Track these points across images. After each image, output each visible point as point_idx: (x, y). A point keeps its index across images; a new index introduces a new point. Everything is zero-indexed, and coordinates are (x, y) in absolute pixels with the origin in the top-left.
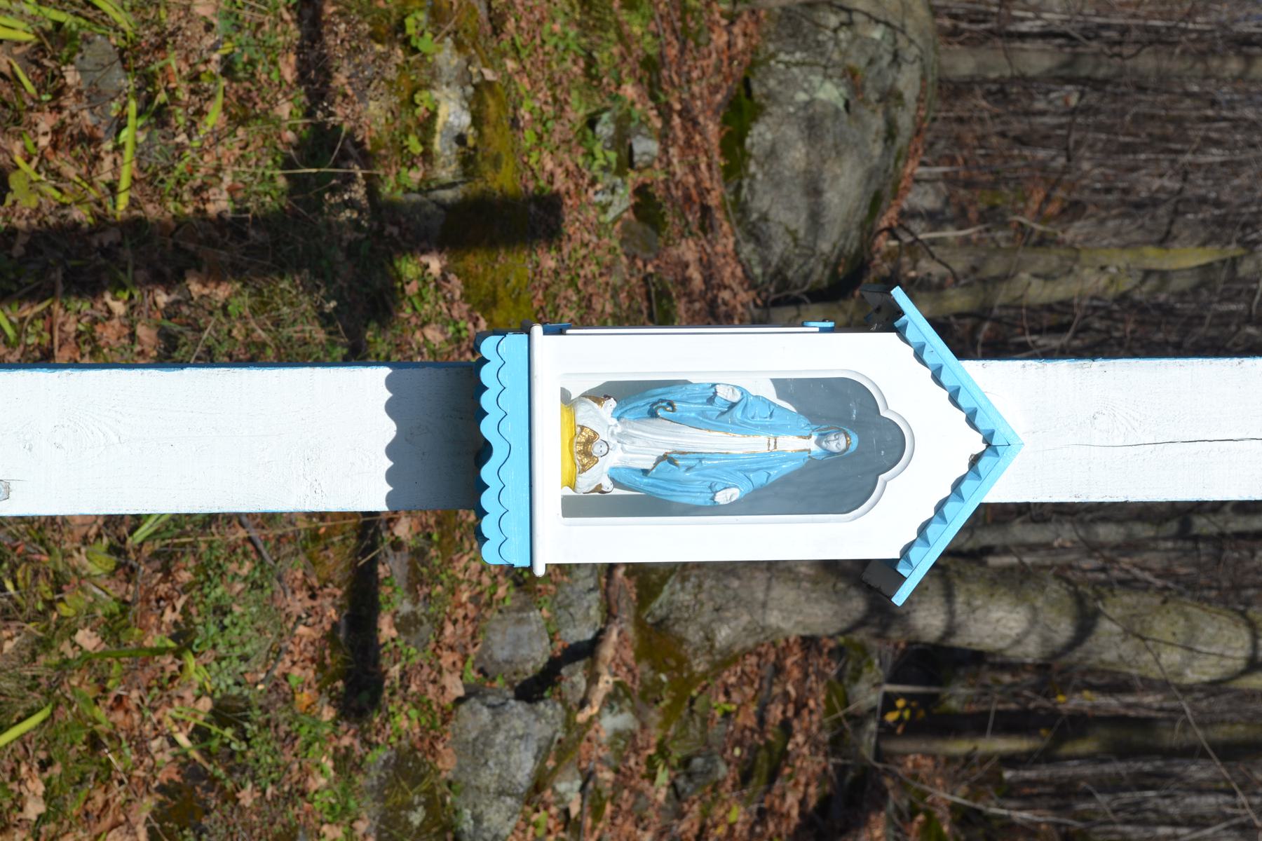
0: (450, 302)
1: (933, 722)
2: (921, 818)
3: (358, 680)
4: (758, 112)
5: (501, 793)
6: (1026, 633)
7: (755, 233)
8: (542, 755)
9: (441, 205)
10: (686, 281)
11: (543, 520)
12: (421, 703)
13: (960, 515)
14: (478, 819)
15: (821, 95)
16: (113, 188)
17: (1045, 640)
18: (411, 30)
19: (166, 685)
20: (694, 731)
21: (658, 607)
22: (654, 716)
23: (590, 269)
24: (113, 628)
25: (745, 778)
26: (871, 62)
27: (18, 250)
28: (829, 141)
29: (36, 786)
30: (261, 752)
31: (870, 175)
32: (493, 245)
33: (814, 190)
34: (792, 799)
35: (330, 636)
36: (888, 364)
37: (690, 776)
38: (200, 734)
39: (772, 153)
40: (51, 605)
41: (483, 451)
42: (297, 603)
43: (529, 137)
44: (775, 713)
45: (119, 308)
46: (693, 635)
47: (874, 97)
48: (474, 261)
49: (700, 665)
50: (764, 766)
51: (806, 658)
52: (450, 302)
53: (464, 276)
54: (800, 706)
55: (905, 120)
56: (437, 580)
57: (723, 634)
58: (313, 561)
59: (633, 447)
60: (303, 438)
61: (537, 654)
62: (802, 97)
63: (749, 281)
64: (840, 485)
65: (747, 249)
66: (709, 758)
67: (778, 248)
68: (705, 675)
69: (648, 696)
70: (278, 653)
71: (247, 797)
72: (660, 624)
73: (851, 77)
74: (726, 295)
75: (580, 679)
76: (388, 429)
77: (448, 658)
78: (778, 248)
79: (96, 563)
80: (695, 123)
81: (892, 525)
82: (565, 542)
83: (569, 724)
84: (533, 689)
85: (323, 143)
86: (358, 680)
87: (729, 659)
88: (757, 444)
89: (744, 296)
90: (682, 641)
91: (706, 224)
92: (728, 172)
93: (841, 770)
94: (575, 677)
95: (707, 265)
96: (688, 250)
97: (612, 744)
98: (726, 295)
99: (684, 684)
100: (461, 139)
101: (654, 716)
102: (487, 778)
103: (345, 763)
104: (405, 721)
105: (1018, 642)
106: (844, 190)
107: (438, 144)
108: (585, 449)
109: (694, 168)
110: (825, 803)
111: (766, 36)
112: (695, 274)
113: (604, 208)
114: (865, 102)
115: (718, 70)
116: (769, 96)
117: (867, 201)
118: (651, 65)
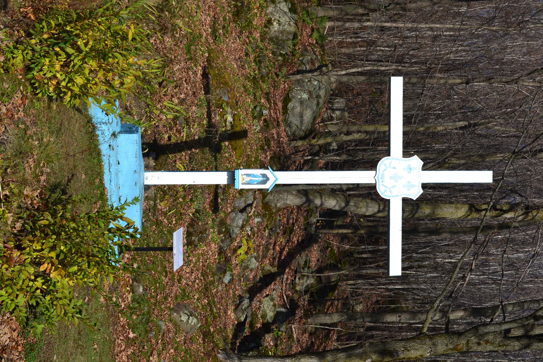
0: (229, 149)
1: (329, 225)
2: (330, 249)
3: (215, 207)
4: (290, 100)
5: (237, 227)
6: (336, 205)
7: (289, 125)
8: (243, 221)
9: (228, 134)
10: (273, 137)
11: (240, 185)
12: (224, 212)
13: (274, 185)
14: (233, 231)
15: (303, 97)
16: (183, 137)
17: (340, 207)
18: (223, 106)
19: (189, 207)
20: (273, 223)
21: (266, 199)
22: (265, 220)
23: (252, 141)
24: (184, 198)
25: (284, 234)
26: (314, 89)
27: (172, 147)
28: (305, 106)
29: (174, 219)
30: (202, 217)
31: (314, 113)
32: (236, 140)
33: (301, 116)
34: (295, 239)
35: (211, 201)
36: (268, 172)
37: (272, 231)
38: (193, 214)
39: (293, 109)
40: (176, 195)
41: (235, 179)
42: (207, 196)
43: (242, 122)
44: (291, 221)
45: (184, 154)
46: (273, 205)
47: (314, 96)
48: (233, 142)
49: (274, 211)
50: (288, 231)
51: (298, 211)
52: (229, 149)
53: (231, 145)
54: (297, 220)
55: (321, 101)
56: (227, 193)
57: (279, 205)
58: (209, 190)
59: (248, 179)
60: (219, 178)
61: (243, 205)
62: (299, 97)
63: (288, 136)
64: (264, 182)
65: (287, 129)
66: (276, 228)
67: (294, 128)
68: (275, 212)
69: (264, 216)
70: (204, 203)
71: (200, 224)
72: (267, 203)
73: (310, 93)
74: (282, 139)
75: (250, 209)
76: (227, 177)
77: (229, 205)
78: (294, 128)
79: (181, 189)
80: (276, 104)
81: (268, 186)
82: (242, 187)
83: (248, 216)
84: (242, 211)
85: (210, 125)
86: (215, 207)
87: (279, 210)
88: (258, 179)
89: (286, 139)
90: (271, 206)
91: (278, 125)
92: (284, 113)
93: (307, 235)
94: (249, 209)
95: (278, 134)
96: (274, 131)
97: (257, 224)
98: (282, 139)
99: (271, 214)
100: (231, 123)
101: (265, 220)
102: (235, 224)
103: (213, 219)
104: (222, 215)
105: (334, 207)
106: (308, 115)
107: (227, 123)
108: (243, 179)
109: (276, 113)
110: (303, 241)
111: (292, 84)
112: (275, 136)
113: (255, 129)
114: (312, 98)
115: (282, 92)
116: (293, 97)
117: (312, 118)
118: (267, 94)
